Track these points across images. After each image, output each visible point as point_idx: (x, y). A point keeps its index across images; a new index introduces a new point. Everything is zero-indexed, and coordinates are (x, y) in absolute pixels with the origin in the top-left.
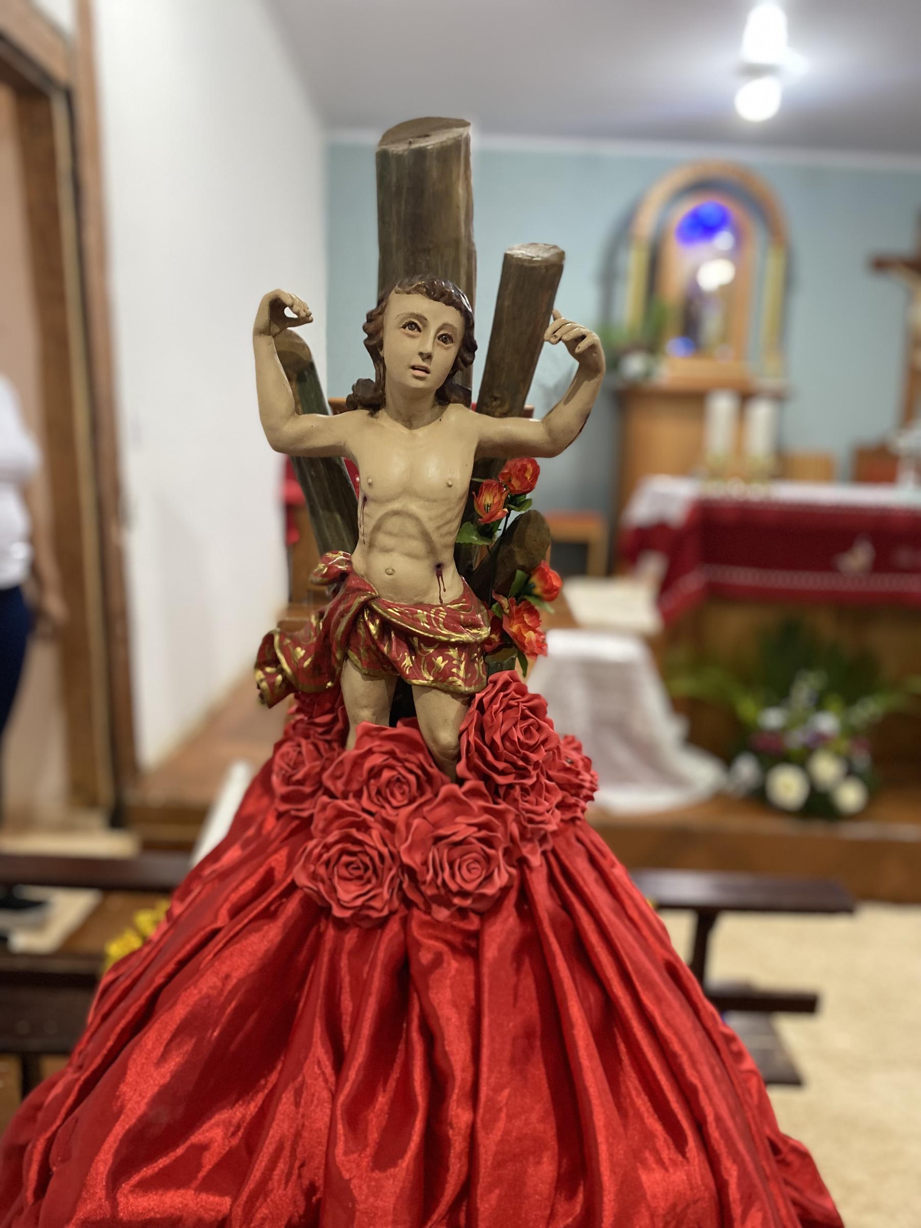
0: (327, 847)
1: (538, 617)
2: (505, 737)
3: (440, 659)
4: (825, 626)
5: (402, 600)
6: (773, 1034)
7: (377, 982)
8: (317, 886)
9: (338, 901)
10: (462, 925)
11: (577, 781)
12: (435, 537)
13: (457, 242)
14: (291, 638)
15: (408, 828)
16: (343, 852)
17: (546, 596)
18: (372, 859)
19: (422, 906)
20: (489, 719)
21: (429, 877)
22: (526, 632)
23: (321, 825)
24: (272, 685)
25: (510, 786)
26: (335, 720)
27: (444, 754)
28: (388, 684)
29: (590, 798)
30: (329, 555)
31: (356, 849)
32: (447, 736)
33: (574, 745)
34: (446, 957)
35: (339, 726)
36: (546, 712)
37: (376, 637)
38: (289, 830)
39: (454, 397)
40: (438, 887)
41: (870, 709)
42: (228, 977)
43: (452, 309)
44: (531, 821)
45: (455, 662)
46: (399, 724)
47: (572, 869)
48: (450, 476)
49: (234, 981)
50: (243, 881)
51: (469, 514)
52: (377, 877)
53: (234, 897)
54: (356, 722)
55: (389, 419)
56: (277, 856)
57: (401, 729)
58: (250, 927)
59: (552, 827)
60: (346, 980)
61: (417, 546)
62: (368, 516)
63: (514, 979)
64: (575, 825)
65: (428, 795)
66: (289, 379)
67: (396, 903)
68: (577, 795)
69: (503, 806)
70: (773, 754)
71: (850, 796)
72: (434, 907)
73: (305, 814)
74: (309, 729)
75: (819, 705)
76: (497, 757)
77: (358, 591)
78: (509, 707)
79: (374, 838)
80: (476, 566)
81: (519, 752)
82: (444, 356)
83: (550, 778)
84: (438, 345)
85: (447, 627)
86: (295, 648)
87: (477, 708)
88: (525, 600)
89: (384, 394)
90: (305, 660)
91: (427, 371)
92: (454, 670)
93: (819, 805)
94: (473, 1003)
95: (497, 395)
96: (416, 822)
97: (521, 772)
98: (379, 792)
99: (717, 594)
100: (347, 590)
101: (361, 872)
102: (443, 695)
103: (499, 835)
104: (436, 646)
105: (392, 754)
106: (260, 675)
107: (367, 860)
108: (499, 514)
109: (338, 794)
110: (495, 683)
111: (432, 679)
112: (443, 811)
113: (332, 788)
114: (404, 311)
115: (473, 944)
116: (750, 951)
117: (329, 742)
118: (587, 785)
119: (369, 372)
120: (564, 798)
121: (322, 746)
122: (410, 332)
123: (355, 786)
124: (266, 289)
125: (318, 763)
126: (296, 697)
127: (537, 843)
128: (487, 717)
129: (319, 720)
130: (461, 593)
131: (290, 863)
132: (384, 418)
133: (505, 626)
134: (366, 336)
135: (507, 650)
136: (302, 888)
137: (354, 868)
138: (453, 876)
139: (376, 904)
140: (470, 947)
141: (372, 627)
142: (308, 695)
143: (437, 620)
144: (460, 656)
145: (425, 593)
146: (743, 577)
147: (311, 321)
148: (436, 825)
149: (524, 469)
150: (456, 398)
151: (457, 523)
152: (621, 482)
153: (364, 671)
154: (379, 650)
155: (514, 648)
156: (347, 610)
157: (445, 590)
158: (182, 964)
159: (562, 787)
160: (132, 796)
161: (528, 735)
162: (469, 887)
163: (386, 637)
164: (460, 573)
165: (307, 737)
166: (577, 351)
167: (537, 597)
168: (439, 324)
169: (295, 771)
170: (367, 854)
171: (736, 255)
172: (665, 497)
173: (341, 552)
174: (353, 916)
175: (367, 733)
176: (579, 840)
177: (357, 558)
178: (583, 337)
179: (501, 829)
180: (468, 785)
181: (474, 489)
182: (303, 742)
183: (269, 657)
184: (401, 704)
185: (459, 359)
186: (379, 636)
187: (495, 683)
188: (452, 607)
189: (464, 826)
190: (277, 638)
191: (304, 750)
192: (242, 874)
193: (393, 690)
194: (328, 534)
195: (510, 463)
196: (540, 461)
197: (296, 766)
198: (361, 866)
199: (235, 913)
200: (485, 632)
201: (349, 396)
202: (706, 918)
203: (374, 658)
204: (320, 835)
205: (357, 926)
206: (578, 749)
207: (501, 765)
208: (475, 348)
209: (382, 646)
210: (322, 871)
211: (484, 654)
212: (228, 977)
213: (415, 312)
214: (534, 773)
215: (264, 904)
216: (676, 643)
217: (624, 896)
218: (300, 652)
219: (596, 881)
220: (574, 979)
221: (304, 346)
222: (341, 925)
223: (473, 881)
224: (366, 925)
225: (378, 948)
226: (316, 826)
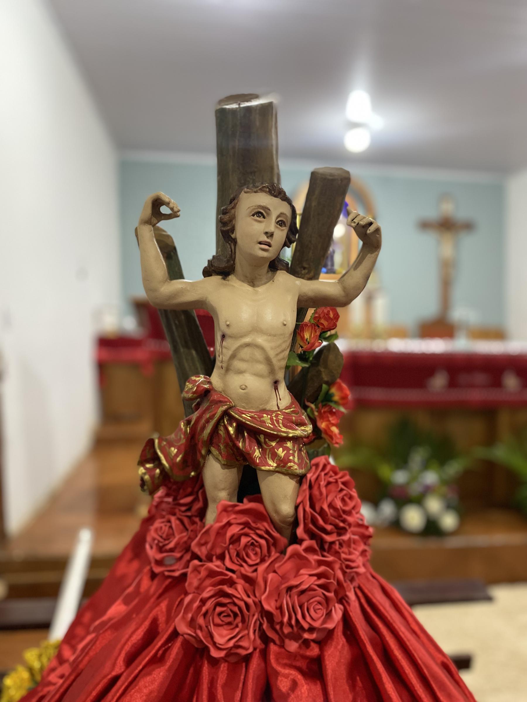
2: (331, 506)
3: (281, 449)
4: (423, 421)
5: (252, 407)
8: (195, 633)
9: (214, 644)
10: (308, 653)
12: (274, 361)
14: (166, 440)
19: (278, 642)
23: (196, 583)
24: (152, 477)
27: (284, 522)
32: (287, 508)
38: (164, 586)
39: (280, 266)
41: (454, 468)
43: (285, 203)
45: (291, 452)
46: (245, 500)
47: (374, 601)
50: (133, 633)
53: (127, 648)
55: (237, 281)
58: (143, 672)
61: (262, 368)
67: (258, 641)
70: (403, 499)
71: (449, 521)
72: (287, 641)
73: (177, 574)
74: (175, 508)
75: (426, 466)
76: (325, 521)
77: (219, 402)
78: (329, 483)
81: (341, 516)
84: (277, 227)
85: (285, 426)
86: (170, 448)
89: (234, 264)
90: (178, 457)
91: (269, 245)
92: (291, 458)
93: (432, 528)
98: (238, 555)
100: (211, 402)
106: (142, 470)
107: (236, 609)
109: (203, 558)
110: (317, 465)
111: (275, 465)
113: (199, 553)
114: (254, 205)
121: (186, 521)
122: (258, 218)
123: (219, 551)
125: (184, 534)
129: (182, 501)
130: (290, 401)
136: (182, 635)
137: (225, 616)
140: (315, 671)
144: (294, 447)
145: (267, 402)
146: (376, 394)
147: (178, 216)
148: (284, 578)
150: (282, 268)
151: (287, 352)
153: (223, 462)
156: (212, 417)
157: (280, 400)
162: (316, 624)
163: (240, 436)
165: (174, 514)
167: (336, 403)
169: (167, 542)
170: (235, 604)
173: (202, 376)
175: (225, 510)
177: (216, 379)
180: (305, 544)
182: (173, 519)
184: (248, 485)
186: (236, 436)
187: (317, 465)
188: (287, 411)
189: (307, 576)
190: (156, 441)
191: (174, 526)
192: (133, 626)
193: (241, 474)
194: (186, 365)
197: (169, 537)
198: (231, 614)
199: (130, 660)
205: (226, 661)
207: (329, 527)
209: (238, 442)
210: (201, 621)
213: (262, 204)
215: (154, 651)
223: (319, 619)
226: (190, 584)
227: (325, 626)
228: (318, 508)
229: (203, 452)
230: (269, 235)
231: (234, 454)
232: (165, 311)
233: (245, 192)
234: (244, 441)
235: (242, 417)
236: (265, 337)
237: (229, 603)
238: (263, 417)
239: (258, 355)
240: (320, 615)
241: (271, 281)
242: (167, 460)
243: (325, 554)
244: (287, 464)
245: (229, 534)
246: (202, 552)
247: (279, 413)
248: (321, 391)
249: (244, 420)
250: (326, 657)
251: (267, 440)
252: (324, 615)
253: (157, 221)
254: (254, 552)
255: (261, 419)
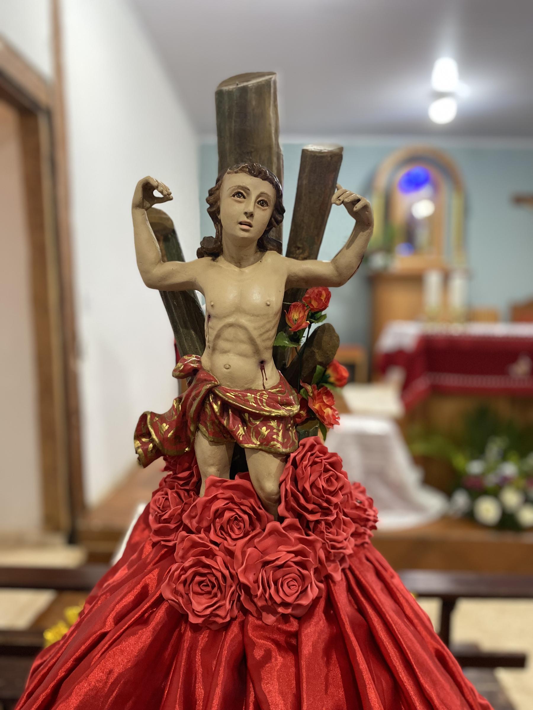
0: (185, 570)
1: (333, 398)
2: (313, 485)
3: (264, 428)
4: (504, 409)
5: (237, 387)
6: (495, 681)
7: (222, 676)
10: (285, 627)
11: (365, 516)
12: (258, 341)
13: (270, 147)
15: (246, 556)
16: (196, 574)
17: (337, 383)
18: (217, 579)
20: (301, 472)
21: (259, 593)
22: (325, 408)
23: (181, 553)
25: (318, 522)
26: (191, 475)
27: (269, 499)
28: (228, 449)
29: (374, 528)
30: (186, 357)
31: (205, 571)
32: (270, 486)
33: (361, 489)
34: (274, 654)
35: (194, 479)
36: (342, 466)
37: (218, 414)
39: (270, 246)
40: (266, 600)
42: (111, 672)
43: (266, 183)
44: (333, 547)
45: (275, 431)
46: (237, 477)
48: (268, 298)
49: (116, 675)
51: (283, 325)
52: (221, 593)
53: (119, 607)
54: (206, 476)
56: (150, 575)
57: (238, 480)
58: (127, 632)
59: (349, 551)
60: (200, 670)
61: (246, 348)
62: (211, 328)
63: (325, 670)
64: (364, 548)
65: (258, 530)
66: (158, 240)
67: (236, 612)
68: (365, 526)
69: (313, 537)
70: (477, 490)
72: (264, 614)
73: (171, 544)
75: (504, 457)
76: (307, 500)
77: (205, 381)
79: (218, 563)
80: (288, 365)
81: (324, 497)
82: (262, 216)
83: (345, 515)
84: (259, 207)
86: (162, 424)
87: (292, 464)
88: (323, 386)
89: (221, 245)
90: (169, 433)
91: (250, 225)
92: (275, 436)
93: (508, 522)
94: (294, 691)
95: (299, 245)
96: (249, 550)
97: (325, 511)
98: (222, 528)
99: (437, 391)
101: (208, 589)
102: (267, 455)
103: (311, 560)
104: (262, 419)
105: (231, 499)
107: (213, 579)
108: (304, 324)
109: (194, 530)
110: (304, 445)
111: (258, 443)
112: (269, 541)
115: (294, 642)
116: (480, 624)
117: (188, 491)
118: (371, 518)
119: (212, 232)
120: (356, 528)
121: (182, 493)
123: (205, 524)
124: (141, 176)
125: (180, 506)
126: (165, 459)
127: (338, 563)
128: (299, 471)
130: (278, 381)
131: (160, 580)
132: (222, 261)
133: (310, 405)
134: (208, 206)
135: (312, 422)
138: (277, 591)
139: (222, 613)
140: (291, 646)
141: (215, 406)
142: (172, 457)
143: (261, 401)
144: (278, 426)
145: (253, 381)
146: (451, 380)
147: (172, 199)
148: (264, 552)
149: (320, 294)
150: (272, 247)
151: (273, 332)
152: (374, 327)
153: (210, 439)
154: (220, 423)
155: (317, 420)
156: (197, 395)
157: (266, 379)
158: (79, 661)
159: (354, 520)
160: (82, 524)
161: (329, 484)
162: (289, 600)
164: (277, 368)
165: (172, 488)
166: (355, 209)
168: (257, 193)
170: (214, 575)
171: (434, 198)
172: (401, 334)
174: (204, 621)
175: (214, 484)
176: (368, 559)
177: (205, 359)
178: (359, 200)
179: (312, 554)
181: (285, 309)
182: (169, 492)
183: (144, 431)
184: (238, 463)
185: (273, 219)
186: (220, 413)
188: (272, 391)
190: (149, 417)
193: (232, 452)
195: (310, 291)
196: (331, 289)
197: (164, 509)
199: (119, 619)
200: (296, 409)
201: (199, 249)
202: (448, 604)
203: (217, 429)
204: (180, 560)
205: (209, 628)
206: (363, 492)
207: (310, 507)
208: (284, 211)
209: (222, 420)
210: (181, 588)
211: (296, 425)
212: (111, 672)
213: (241, 185)
214: (334, 512)
216: (413, 422)
217: (402, 600)
218: (165, 427)
219: (382, 590)
220: (368, 664)
221: (169, 219)
222: (196, 628)
223: (292, 595)
224: (214, 627)
225: (222, 648)
227: (299, 602)
228: (300, 488)
229: (192, 428)
230: (248, 215)
231: (221, 431)
232: (173, 292)
233: (228, 173)
234: (229, 419)
235: (227, 396)
236: (248, 317)
237: (208, 573)
238: (247, 396)
239: (242, 335)
240: (294, 591)
241: (259, 262)
242: (156, 435)
243: (310, 533)
244: (270, 442)
245: (214, 508)
246: (193, 524)
247: (264, 392)
248: (315, 372)
249: (227, 399)
250: (303, 634)
251: (251, 419)
252: (299, 592)
253: (149, 205)
254: (239, 527)
255: (245, 398)
